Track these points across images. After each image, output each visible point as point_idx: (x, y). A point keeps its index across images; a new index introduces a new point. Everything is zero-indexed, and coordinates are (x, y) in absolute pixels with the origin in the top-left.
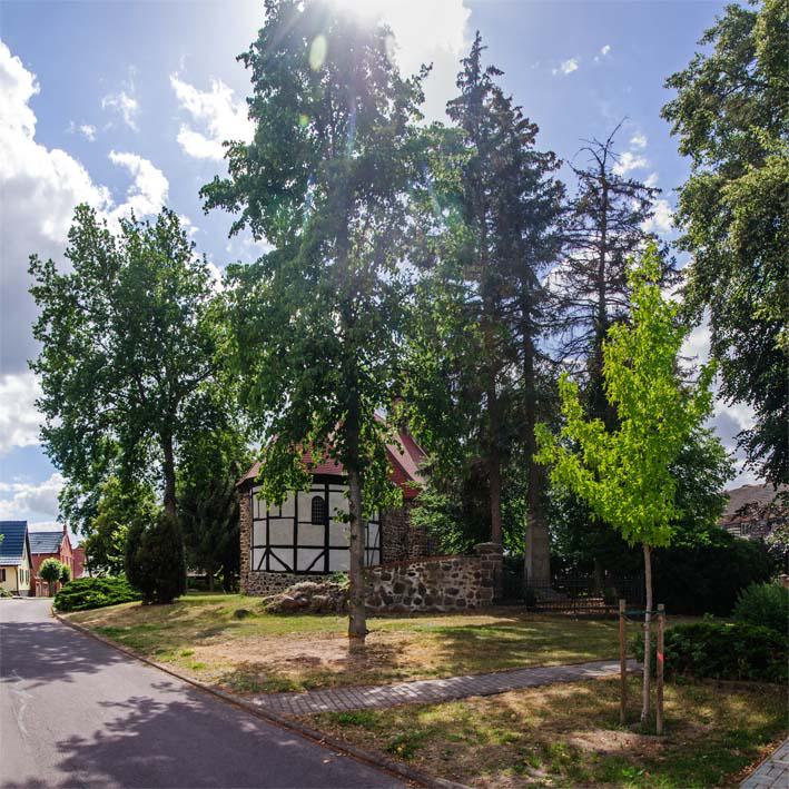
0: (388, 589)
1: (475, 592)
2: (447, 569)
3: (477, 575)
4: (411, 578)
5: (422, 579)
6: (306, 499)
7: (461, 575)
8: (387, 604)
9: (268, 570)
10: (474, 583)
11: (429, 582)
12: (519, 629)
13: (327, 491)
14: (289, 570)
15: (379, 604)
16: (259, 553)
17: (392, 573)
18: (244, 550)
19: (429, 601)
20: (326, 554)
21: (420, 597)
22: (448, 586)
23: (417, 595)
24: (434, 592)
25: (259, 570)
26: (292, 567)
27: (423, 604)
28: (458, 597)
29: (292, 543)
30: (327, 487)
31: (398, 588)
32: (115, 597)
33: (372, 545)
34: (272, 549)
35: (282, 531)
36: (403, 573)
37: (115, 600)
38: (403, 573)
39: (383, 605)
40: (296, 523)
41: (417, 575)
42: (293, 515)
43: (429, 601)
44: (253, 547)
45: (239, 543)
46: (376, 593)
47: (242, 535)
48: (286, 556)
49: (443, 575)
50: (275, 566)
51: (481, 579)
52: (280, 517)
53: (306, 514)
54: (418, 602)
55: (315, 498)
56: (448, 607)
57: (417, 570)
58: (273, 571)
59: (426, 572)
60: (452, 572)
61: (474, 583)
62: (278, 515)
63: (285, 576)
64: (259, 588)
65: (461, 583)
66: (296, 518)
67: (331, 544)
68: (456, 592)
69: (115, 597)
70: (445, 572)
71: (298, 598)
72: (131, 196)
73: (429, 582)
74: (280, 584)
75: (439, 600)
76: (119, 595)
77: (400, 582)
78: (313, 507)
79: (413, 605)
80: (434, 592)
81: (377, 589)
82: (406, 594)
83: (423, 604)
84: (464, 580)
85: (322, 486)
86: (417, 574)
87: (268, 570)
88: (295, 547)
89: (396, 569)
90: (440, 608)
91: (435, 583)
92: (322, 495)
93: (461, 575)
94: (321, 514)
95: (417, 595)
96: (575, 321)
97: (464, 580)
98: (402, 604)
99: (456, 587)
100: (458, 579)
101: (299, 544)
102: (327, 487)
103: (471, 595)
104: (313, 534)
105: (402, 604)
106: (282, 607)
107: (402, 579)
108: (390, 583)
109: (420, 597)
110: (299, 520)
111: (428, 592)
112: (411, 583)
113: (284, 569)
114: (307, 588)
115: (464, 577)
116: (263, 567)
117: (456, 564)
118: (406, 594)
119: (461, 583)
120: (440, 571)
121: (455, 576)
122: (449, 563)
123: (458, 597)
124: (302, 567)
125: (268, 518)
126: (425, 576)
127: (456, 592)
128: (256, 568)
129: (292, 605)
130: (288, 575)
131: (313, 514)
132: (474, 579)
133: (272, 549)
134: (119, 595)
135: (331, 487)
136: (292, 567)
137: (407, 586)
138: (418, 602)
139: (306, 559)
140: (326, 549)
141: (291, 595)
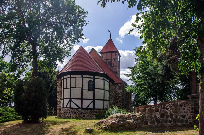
0: (158, 116)
1: (191, 116)
2: (181, 106)
3: (192, 109)
4: (167, 111)
5: (171, 111)
6: (86, 81)
7: (186, 109)
8: (158, 123)
9: (70, 107)
11: (174, 112)
13: (94, 78)
14: (79, 108)
15: (155, 123)
16: (66, 101)
17: (159, 108)
18: (58, 100)
19: (175, 121)
20: (94, 102)
21: (171, 119)
22: (182, 114)
23: (170, 119)
24: (176, 117)
25: (66, 107)
26: (80, 107)
27: (172, 123)
28: (185, 119)
29: (80, 97)
30: (94, 77)
31: (162, 116)
32: (5, 118)
33: (108, 99)
34: (73, 100)
35: (76, 93)
36: (164, 108)
37: (6, 120)
38: (164, 108)
39: (156, 124)
40: (82, 90)
41: (169, 109)
42: (81, 87)
43: (175, 121)
44: (63, 99)
45: (56, 97)
46: (153, 118)
47: (58, 94)
48: (78, 102)
50: (73, 106)
51: (194, 110)
52: (76, 87)
53: (86, 87)
54: (170, 122)
56: (182, 123)
58: (72, 108)
59: (173, 108)
60: (183, 107)
62: (75, 87)
63: (78, 110)
64: (67, 114)
65: (186, 112)
66: (82, 88)
67: (95, 98)
68: (184, 117)
69: (5, 118)
70: (180, 108)
71: (118, 122)
73: (174, 112)
74: (76, 113)
75: (178, 121)
76: (8, 117)
77: (163, 113)
78: (89, 84)
79: (168, 123)
80: (176, 117)
81: (153, 116)
82: (165, 118)
83: (172, 123)
84: (187, 111)
85: (93, 77)
87: (70, 107)
88: (82, 99)
89: (161, 107)
90: (179, 124)
91: (177, 112)
92: (92, 80)
93: (186, 109)
94: (92, 87)
95: (170, 119)
97: (187, 111)
98: (164, 123)
99: (184, 114)
100: (185, 110)
101: (103, 99)
102: (94, 77)
103: (190, 118)
104: (88, 94)
105: (164, 123)
106: (111, 127)
107: (164, 111)
108: (158, 113)
109: (171, 119)
111: (174, 117)
112: (167, 113)
113: (77, 107)
114: (121, 116)
115: (188, 110)
116: (68, 106)
117: (184, 103)
118: (165, 118)
119: (186, 112)
121: (184, 109)
122: (182, 103)
123: (185, 119)
124: (85, 106)
125: (71, 88)
126: (172, 109)
127: (184, 117)
128: (65, 106)
129: (116, 126)
130: (79, 109)
131: (89, 87)
132: (191, 110)
133: (73, 100)
134: (8, 117)
135: (96, 77)
136: (80, 107)
137: (166, 114)
138: (170, 122)
139: (86, 103)
140: (94, 100)
141: (115, 121)
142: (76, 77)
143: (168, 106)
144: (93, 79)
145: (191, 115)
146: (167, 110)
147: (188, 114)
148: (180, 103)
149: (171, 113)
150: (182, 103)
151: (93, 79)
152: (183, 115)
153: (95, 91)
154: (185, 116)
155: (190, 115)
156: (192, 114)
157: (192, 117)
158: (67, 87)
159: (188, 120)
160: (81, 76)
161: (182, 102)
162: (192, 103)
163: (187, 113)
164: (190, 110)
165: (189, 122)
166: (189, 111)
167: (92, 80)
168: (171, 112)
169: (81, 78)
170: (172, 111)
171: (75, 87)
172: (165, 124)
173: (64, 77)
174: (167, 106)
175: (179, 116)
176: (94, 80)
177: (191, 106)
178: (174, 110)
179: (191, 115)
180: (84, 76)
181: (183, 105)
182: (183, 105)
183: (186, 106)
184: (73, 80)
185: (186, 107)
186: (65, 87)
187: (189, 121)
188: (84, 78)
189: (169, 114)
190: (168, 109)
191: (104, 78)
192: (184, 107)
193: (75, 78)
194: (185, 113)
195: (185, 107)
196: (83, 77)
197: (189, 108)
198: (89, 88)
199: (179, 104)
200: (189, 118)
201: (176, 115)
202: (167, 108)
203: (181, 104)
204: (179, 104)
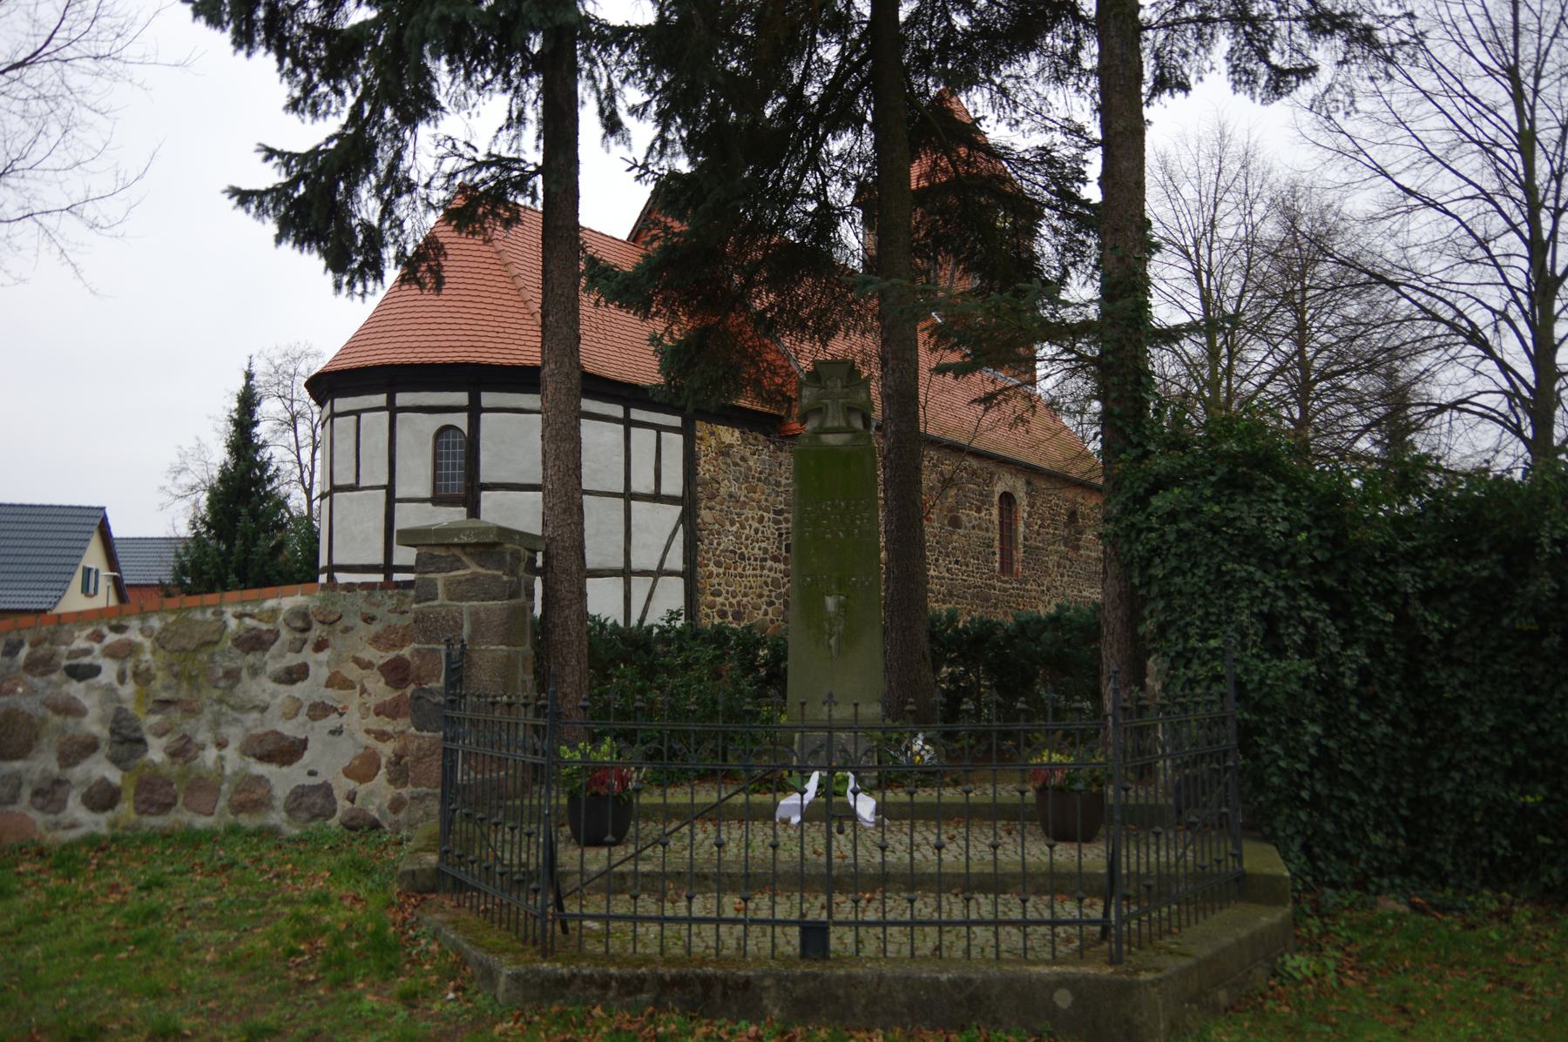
1: (386, 750)
2: (255, 642)
3: (396, 673)
4: (76, 689)
6: (418, 432)
10: (380, 711)
12: (950, 795)
13: (474, 411)
21: (114, 776)
24: (183, 751)
40: (391, 501)
42: (384, 481)
49: (232, 676)
53: (416, 477)
55: (444, 430)
57: (111, 653)
60: (278, 659)
61: (380, 711)
62: (352, 481)
65: (320, 710)
66: (390, 489)
68: (287, 752)
72: (1091, 301)
78: (436, 456)
80: (183, 751)
84: (331, 696)
85: (461, 398)
86: (109, 671)
95: (99, 768)
96: (1076, 33)
97: (331, 696)
99: (290, 729)
103: (363, 769)
109: (114, 776)
110: (400, 493)
111: (156, 752)
112: (80, 712)
115: (336, 681)
119: (320, 710)
120: (228, 658)
121: (295, 675)
126: (143, 677)
131: (436, 477)
132: (379, 690)
135: (487, 399)
138: (102, 798)
142: (357, 413)
143: (97, 647)
144: (464, 416)
145: (382, 736)
146: (82, 685)
147: (337, 732)
148: (251, 616)
149: (119, 710)
150: (274, 612)
151: (464, 416)
152: (275, 733)
153: (483, 504)
154: (306, 740)
155: (370, 741)
156: (388, 725)
157: (390, 763)
158: (362, 484)
159: (339, 794)
160: (380, 399)
161: (270, 603)
162: (394, 619)
163: (333, 721)
164: (363, 691)
165: (343, 805)
166: (353, 699)
167: (461, 421)
168: (130, 706)
169: (385, 415)
170: (140, 699)
171: (352, 481)
172: (35, 815)
173: (337, 401)
174: (80, 643)
175: (221, 745)
176: (474, 424)
177: (376, 641)
178: (157, 685)
179: (382, 736)
180: (403, 399)
181: (285, 635)
182: (285, 635)
183: (320, 646)
184: (643, 440)
185: (324, 656)
186: (345, 477)
187: (352, 797)
188: (400, 416)
189: (93, 725)
190: (94, 671)
191: (627, 413)
192: (292, 659)
193: (354, 418)
194: (302, 718)
195: (308, 655)
196: (393, 409)
197: (351, 671)
198: (435, 487)
199: (233, 623)
200: (349, 772)
201: (187, 739)
202: (86, 660)
203: (264, 627)
204: (233, 623)
